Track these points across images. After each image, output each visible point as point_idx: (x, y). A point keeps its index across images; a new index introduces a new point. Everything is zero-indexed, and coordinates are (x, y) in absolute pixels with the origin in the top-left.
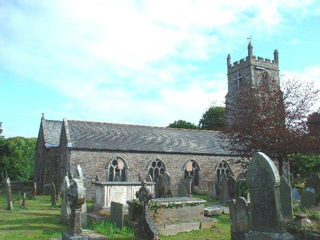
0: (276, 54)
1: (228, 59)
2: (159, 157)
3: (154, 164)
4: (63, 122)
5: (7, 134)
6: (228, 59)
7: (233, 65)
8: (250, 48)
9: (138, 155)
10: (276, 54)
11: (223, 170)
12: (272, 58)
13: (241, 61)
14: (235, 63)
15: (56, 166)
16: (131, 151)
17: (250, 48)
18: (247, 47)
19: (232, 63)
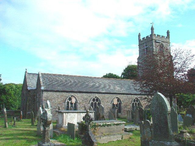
0: (168, 33)
1: (139, 36)
2: (97, 95)
3: (94, 100)
4: (39, 74)
5: (4, 82)
6: (139, 36)
7: (142, 40)
8: (152, 29)
9: (84, 94)
10: (168, 33)
11: (136, 103)
12: (166, 35)
13: (147, 37)
14: (143, 39)
15: (34, 101)
16: (80, 92)
17: (152, 29)
18: (151, 28)
19: (141, 38)
